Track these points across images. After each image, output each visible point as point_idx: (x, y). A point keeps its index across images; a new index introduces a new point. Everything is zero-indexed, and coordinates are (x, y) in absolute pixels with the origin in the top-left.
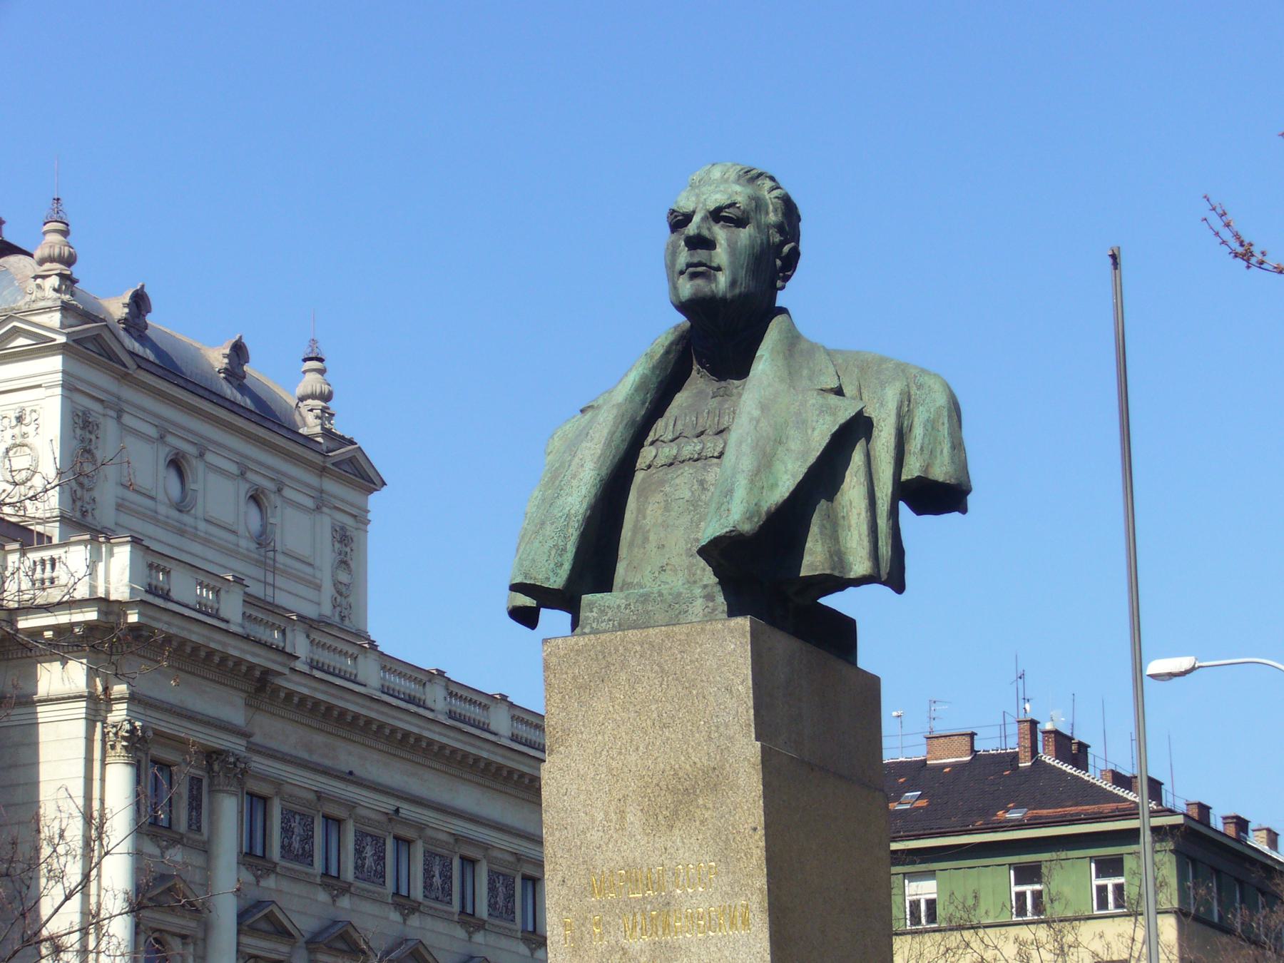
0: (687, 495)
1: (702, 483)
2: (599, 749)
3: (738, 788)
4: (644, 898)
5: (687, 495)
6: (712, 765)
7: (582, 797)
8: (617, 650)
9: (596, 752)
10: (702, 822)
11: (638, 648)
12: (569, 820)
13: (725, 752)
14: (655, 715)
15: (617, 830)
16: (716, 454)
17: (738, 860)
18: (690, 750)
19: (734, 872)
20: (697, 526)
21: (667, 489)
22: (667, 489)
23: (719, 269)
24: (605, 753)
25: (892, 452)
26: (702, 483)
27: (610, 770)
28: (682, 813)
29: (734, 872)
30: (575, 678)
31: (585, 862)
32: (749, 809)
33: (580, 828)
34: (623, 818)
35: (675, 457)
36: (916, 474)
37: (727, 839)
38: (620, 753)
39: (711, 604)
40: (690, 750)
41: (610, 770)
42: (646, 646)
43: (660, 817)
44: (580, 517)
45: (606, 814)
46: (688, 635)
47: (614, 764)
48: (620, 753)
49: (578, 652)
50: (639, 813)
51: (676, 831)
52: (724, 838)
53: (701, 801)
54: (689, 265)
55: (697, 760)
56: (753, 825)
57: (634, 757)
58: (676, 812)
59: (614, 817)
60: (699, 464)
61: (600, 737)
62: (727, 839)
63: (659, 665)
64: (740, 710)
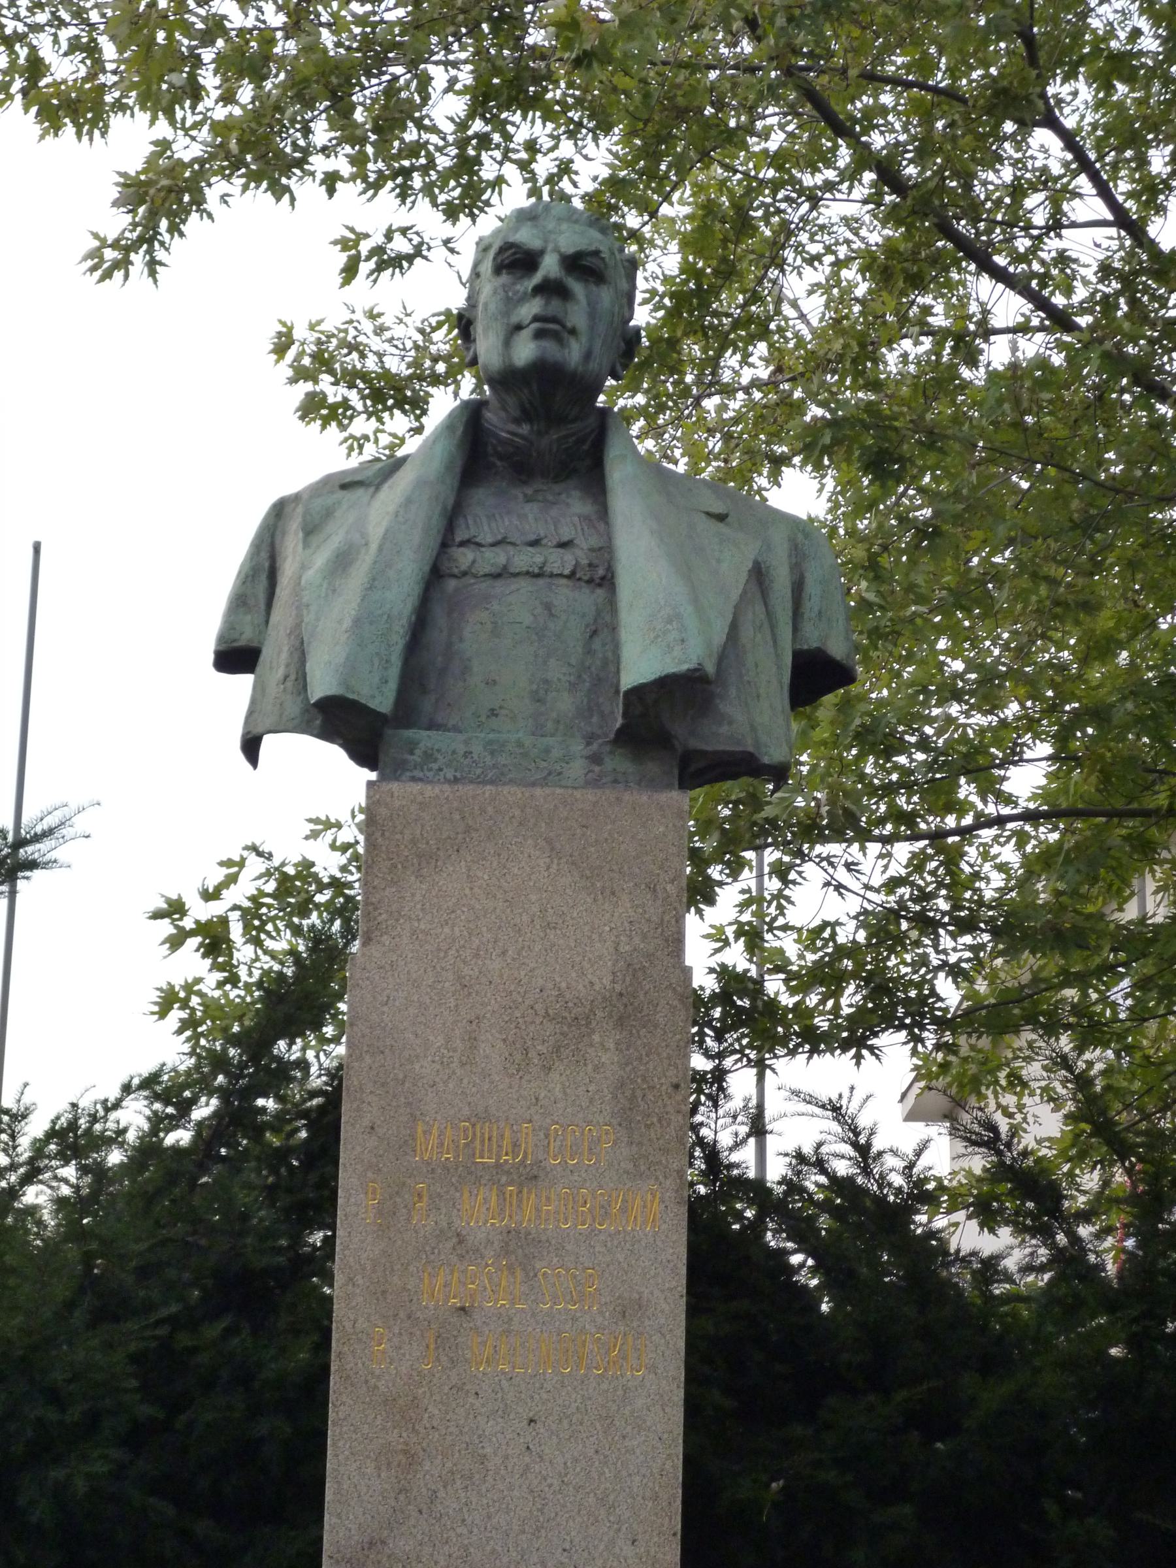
0: (528, 620)
1: (548, 607)
2: (444, 946)
3: (656, 1026)
4: (497, 1165)
5: (528, 620)
6: (618, 988)
7: (412, 1011)
8: (483, 811)
9: (439, 950)
10: (596, 1069)
11: (517, 813)
12: (388, 1042)
13: (640, 974)
14: (535, 909)
15: (463, 1065)
16: (566, 572)
17: (648, 1127)
18: (586, 964)
19: (640, 1144)
20: (545, 663)
21: (496, 607)
22: (496, 607)
23: (573, 332)
24: (452, 952)
25: (789, 605)
26: (548, 607)
27: (460, 978)
28: (565, 1053)
29: (640, 1144)
30: (414, 841)
31: (409, 1104)
32: (669, 1057)
33: (406, 1054)
34: (474, 1048)
35: (505, 567)
36: (815, 645)
37: (634, 1096)
38: (477, 956)
39: (597, 769)
40: (586, 964)
41: (460, 978)
42: (528, 810)
43: (532, 1054)
44: (404, 621)
45: (448, 1040)
46: (595, 804)
47: (466, 971)
48: (477, 956)
49: (423, 806)
50: (500, 1044)
51: (554, 1076)
52: (628, 1093)
53: (596, 1038)
54: (536, 319)
55: (595, 980)
56: (675, 1080)
57: (495, 965)
58: (557, 1049)
59: (458, 1043)
60: (541, 582)
61: (447, 930)
62: (634, 1096)
63: (549, 841)
64: (667, 918)
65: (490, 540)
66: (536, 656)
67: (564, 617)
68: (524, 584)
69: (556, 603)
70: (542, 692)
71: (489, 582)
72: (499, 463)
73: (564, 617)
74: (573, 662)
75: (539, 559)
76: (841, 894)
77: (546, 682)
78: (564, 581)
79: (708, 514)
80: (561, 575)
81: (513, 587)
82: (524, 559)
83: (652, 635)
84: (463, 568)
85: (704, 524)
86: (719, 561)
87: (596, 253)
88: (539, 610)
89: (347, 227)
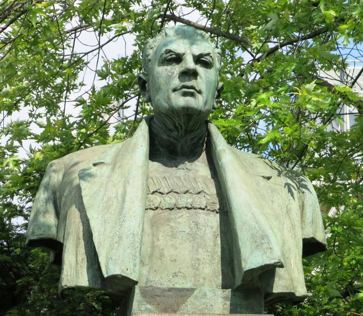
0: (188, 230)
1: (197, 224)
5: (188, 230)
20: (197, 251)
22: (173, 224)
23: (200, 92)
60: (192, 211)
65: (166, 191)
66: (193, 247)
67: (204, 229)
68: (184, 212)
69: (199, 221)
70: (197, 265)
71: (169, 211)
72: (161, 149)
73: (204, 229)
74: (209, 250)
75: (190, 201)
76: (126, 108)
77: (198, 259)
78: (201, 211)
79: (263, 177)
80: (201, 208)
81: (180, 215)
82: (185, 200)
83: (255, 245)
84: (156, 205)
85: (263, 182)
86: (272, 202)
87: (208, 54)
88: (192, 225)
89: (129, 107)
